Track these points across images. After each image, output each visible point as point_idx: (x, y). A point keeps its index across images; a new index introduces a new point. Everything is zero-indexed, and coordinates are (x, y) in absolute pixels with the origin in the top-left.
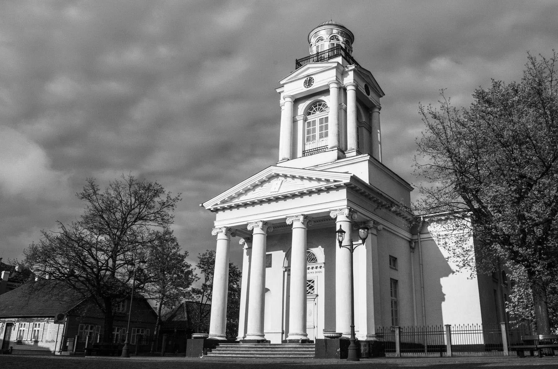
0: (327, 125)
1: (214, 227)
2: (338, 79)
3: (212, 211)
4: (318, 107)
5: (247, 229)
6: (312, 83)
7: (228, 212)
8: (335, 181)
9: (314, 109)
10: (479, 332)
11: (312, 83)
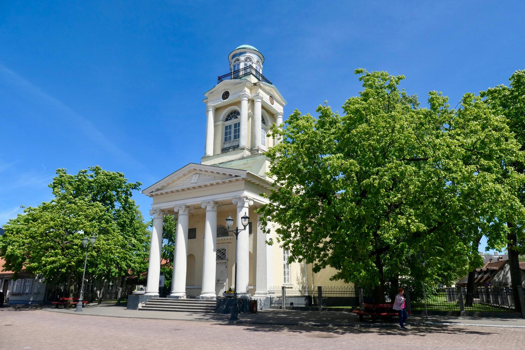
0: (231, 131)
4: (233, 115)
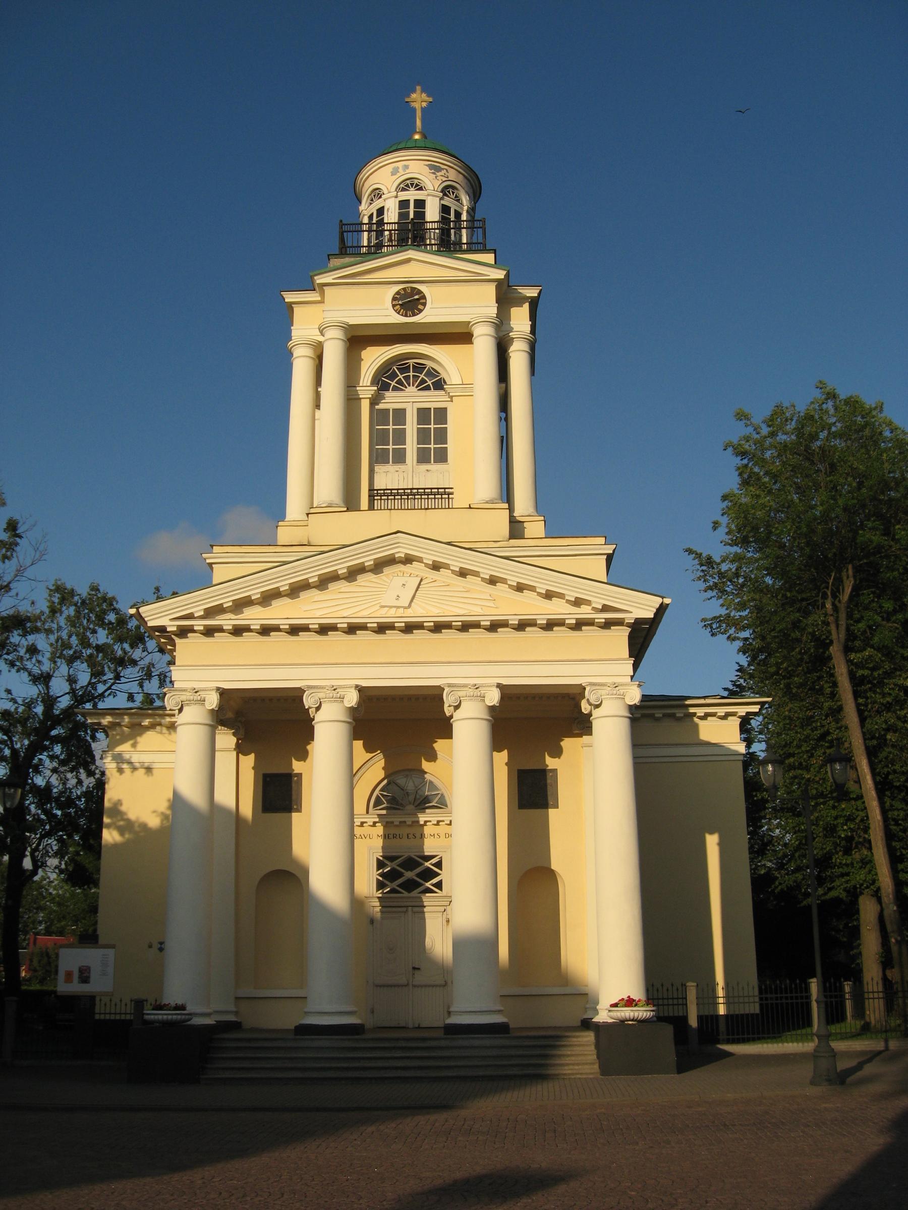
6: (420, 307)
10: (751, 999)
11: (420, 307)
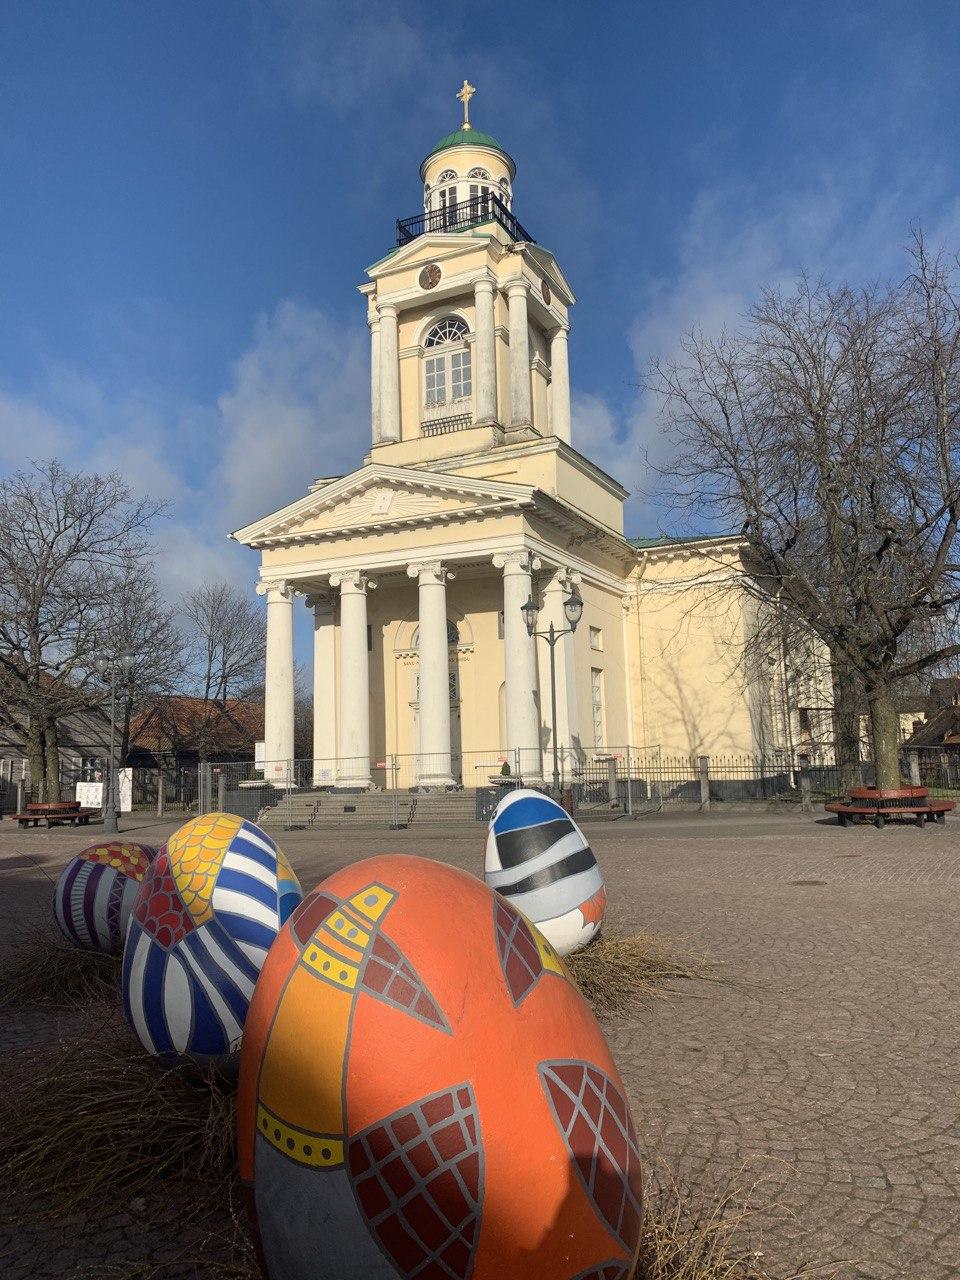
1: (260, 579)
2: (491, 274)
3: (252, 547)
4: (448, 329)
5: (255, 592)
7: (280, 551)
8: (503, 499)
9: (441, 333)
